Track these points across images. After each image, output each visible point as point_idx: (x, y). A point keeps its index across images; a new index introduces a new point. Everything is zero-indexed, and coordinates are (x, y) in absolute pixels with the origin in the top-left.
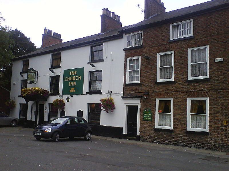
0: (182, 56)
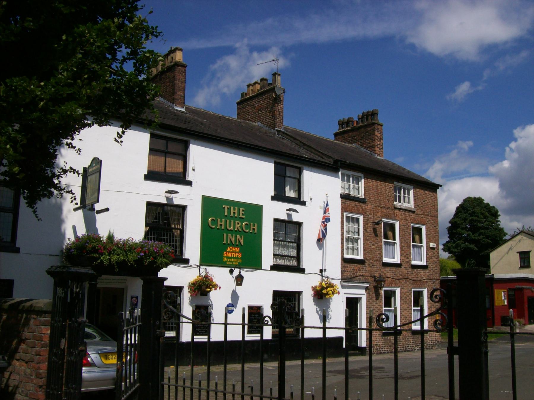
0: (406, 231)
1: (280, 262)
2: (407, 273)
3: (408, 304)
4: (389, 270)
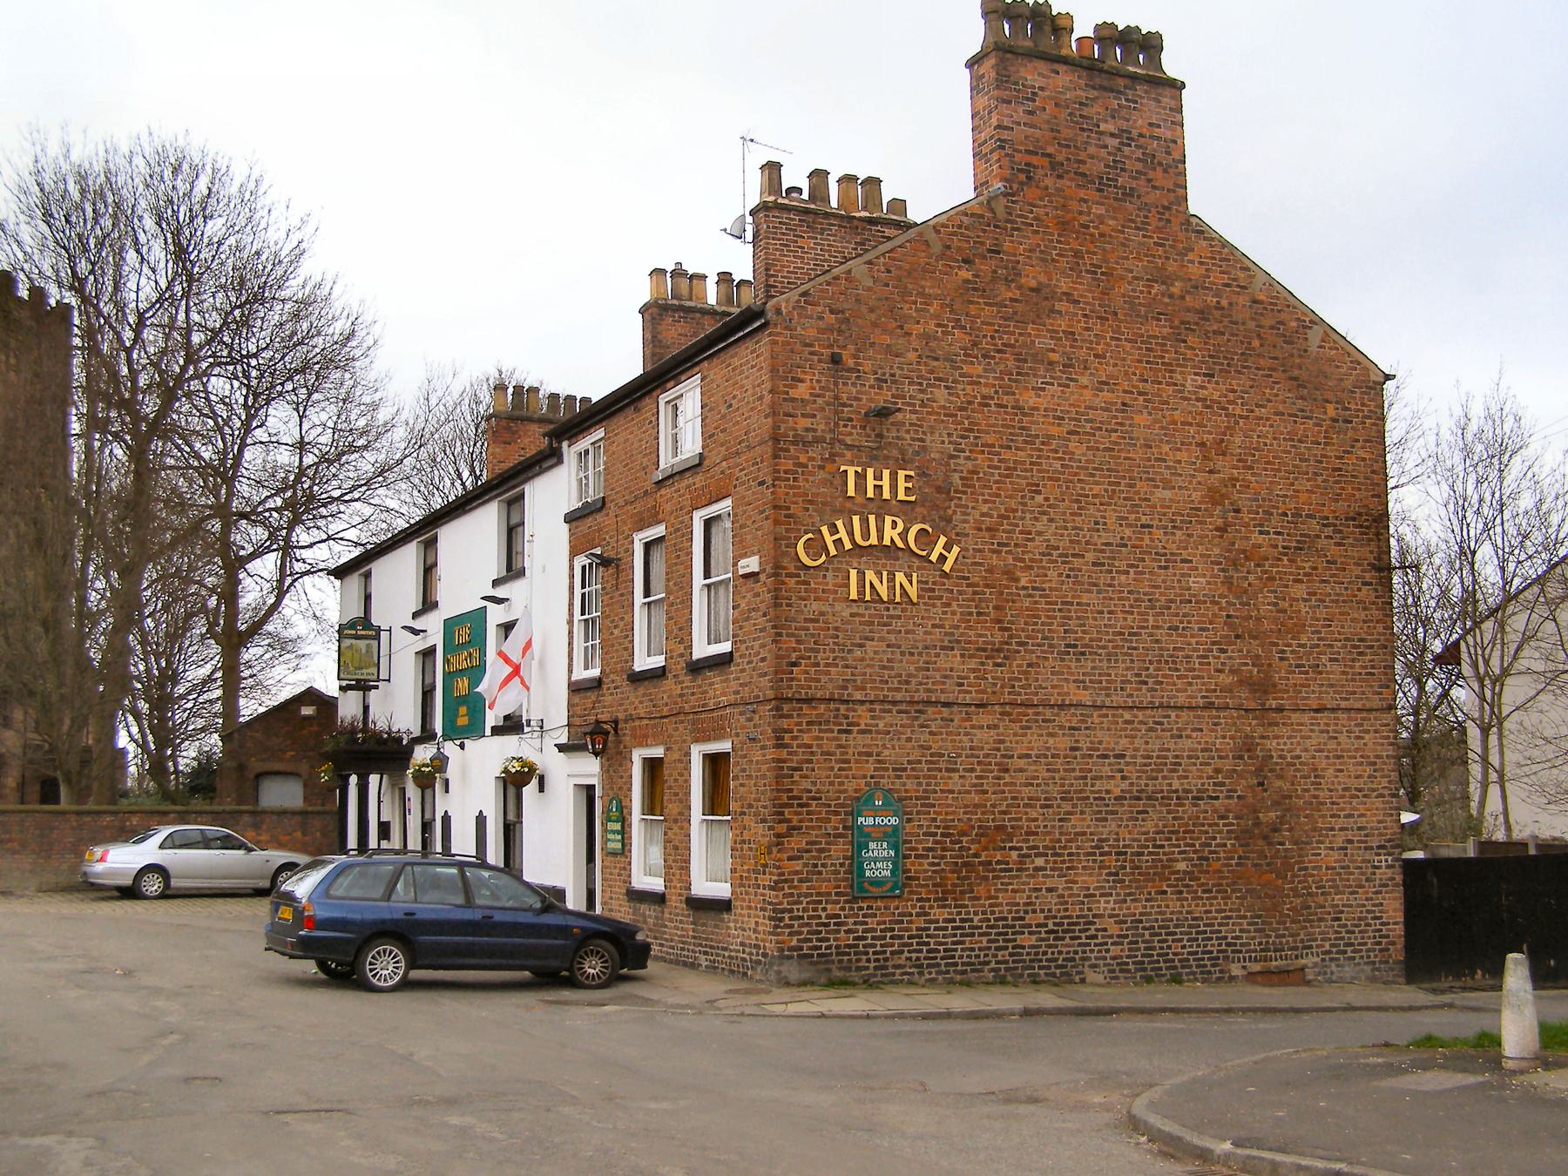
2: (681, 695)
4: (644, 695)
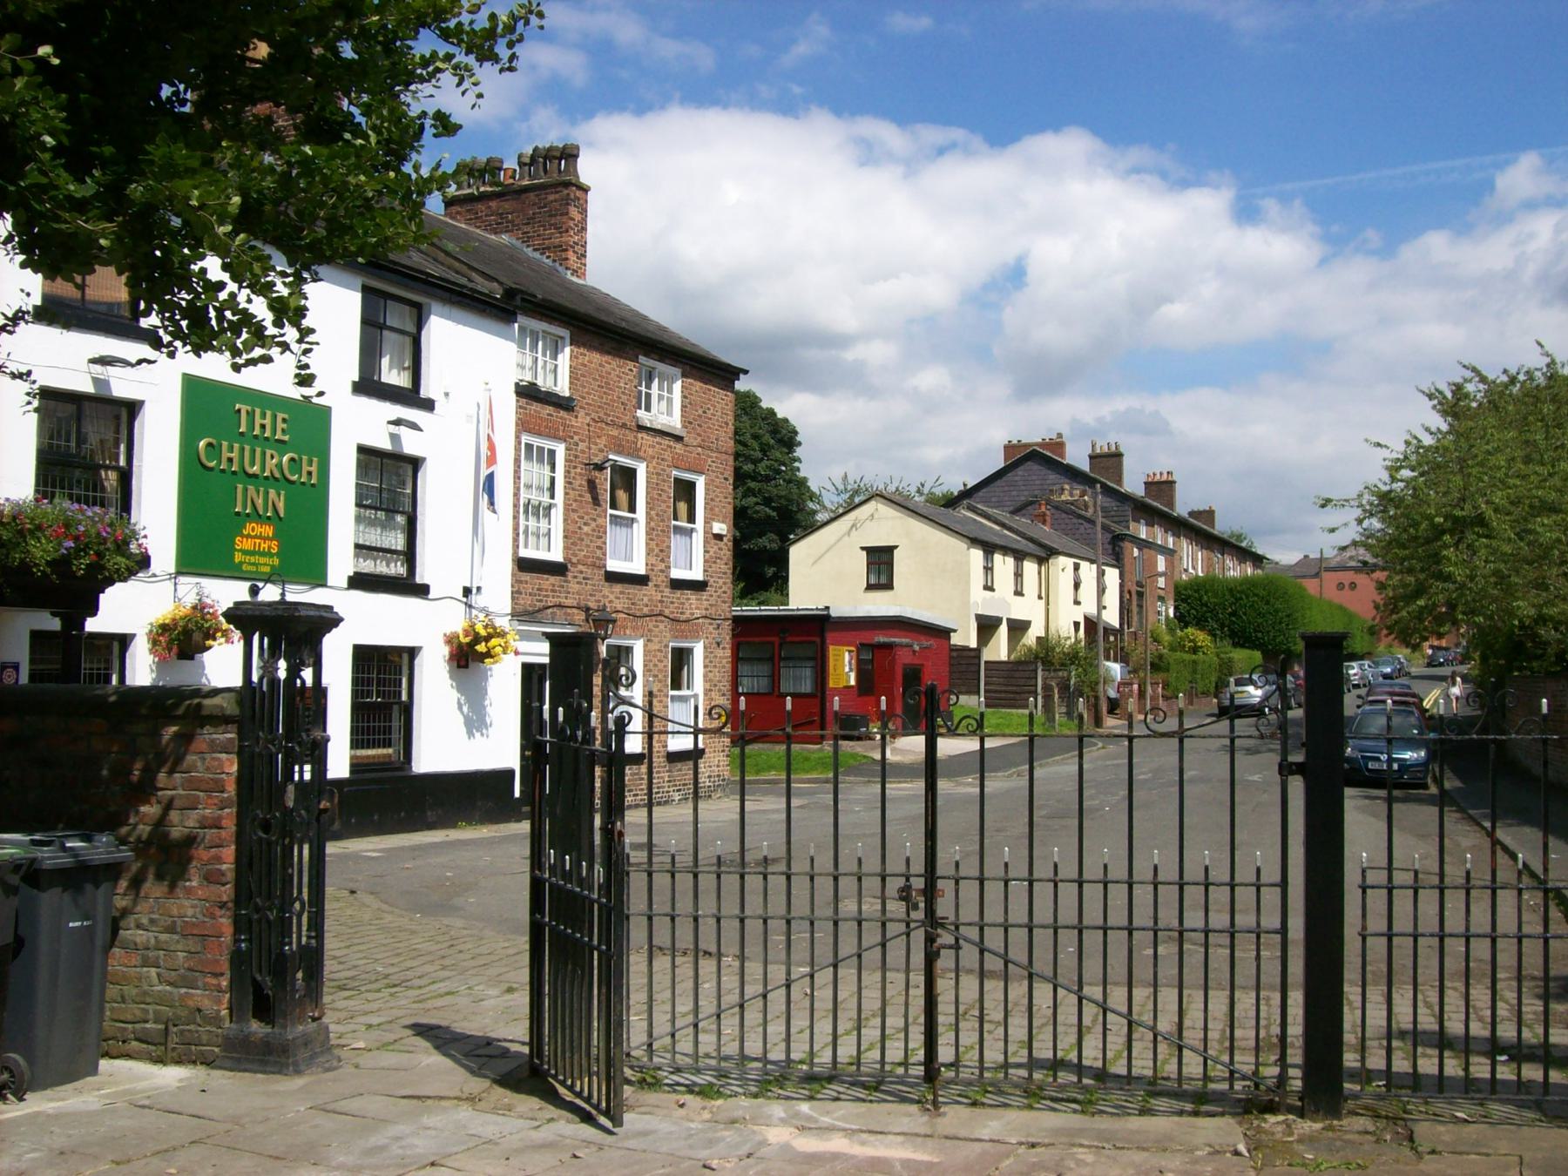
1: (368, 566)
2: (661, 602)
3: (660, 681)
4: (621, 593)
